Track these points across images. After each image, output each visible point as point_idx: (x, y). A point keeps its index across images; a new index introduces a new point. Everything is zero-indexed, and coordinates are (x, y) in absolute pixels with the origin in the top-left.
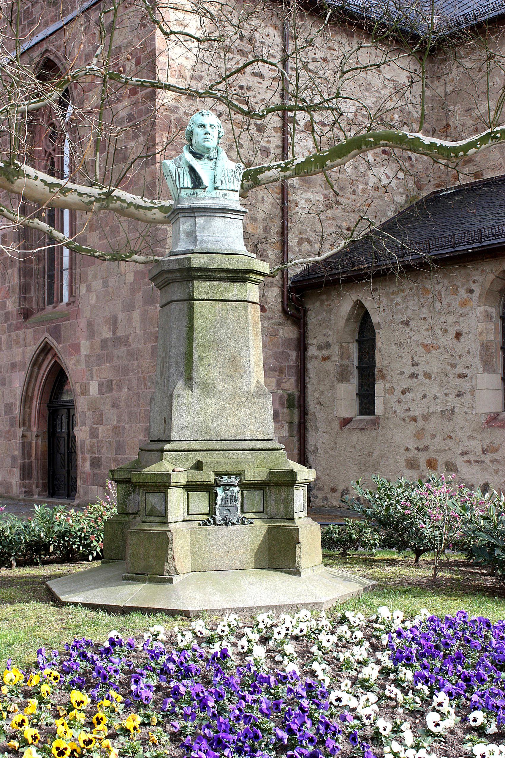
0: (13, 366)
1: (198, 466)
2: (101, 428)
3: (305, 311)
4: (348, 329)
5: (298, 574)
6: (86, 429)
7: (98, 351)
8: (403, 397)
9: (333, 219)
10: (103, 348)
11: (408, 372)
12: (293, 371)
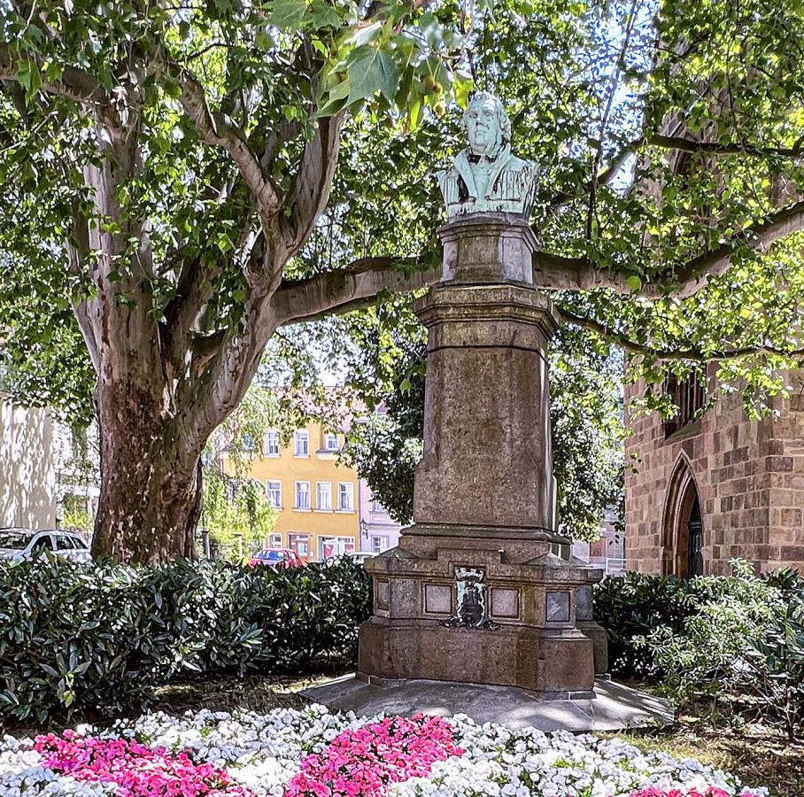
0: (658, 483)
2: (722, 547)
6: (710, 548)
10: (726, 462)
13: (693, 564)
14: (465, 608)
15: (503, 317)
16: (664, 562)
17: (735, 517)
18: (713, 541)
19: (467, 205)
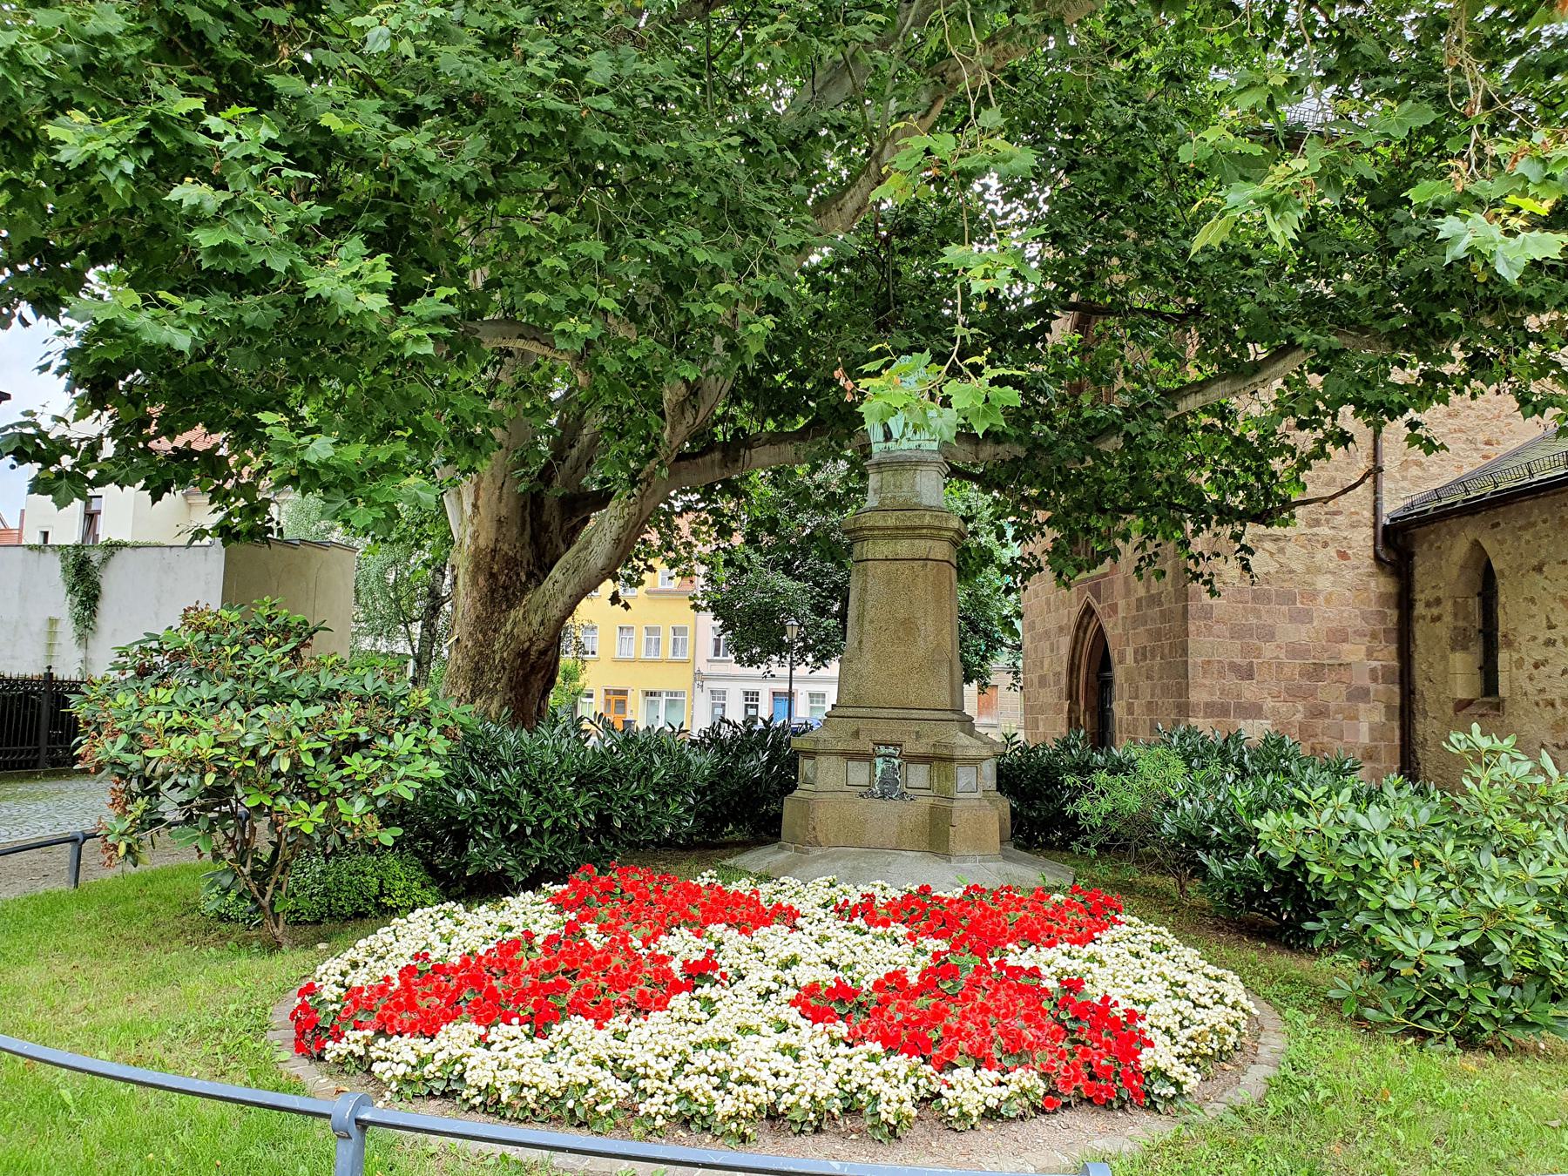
0: (1061, 629)
1: (856, 734)
3: (1411, 555)
4: (1463, 578)
5: (31, 492)
7: (1134, 612)
8: (1535, 672)
9: (1461, 431)
10: (1139, 608)
11: (1541, 640)
12: (1394, 635)
13: (1102, 736)
14: (883, 781)
15: (920, 537)
16: (1070, 719)
17: (1150, 669)
18: (1126, 696)
19: (889, 444)
